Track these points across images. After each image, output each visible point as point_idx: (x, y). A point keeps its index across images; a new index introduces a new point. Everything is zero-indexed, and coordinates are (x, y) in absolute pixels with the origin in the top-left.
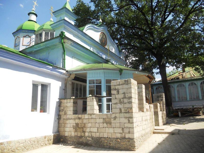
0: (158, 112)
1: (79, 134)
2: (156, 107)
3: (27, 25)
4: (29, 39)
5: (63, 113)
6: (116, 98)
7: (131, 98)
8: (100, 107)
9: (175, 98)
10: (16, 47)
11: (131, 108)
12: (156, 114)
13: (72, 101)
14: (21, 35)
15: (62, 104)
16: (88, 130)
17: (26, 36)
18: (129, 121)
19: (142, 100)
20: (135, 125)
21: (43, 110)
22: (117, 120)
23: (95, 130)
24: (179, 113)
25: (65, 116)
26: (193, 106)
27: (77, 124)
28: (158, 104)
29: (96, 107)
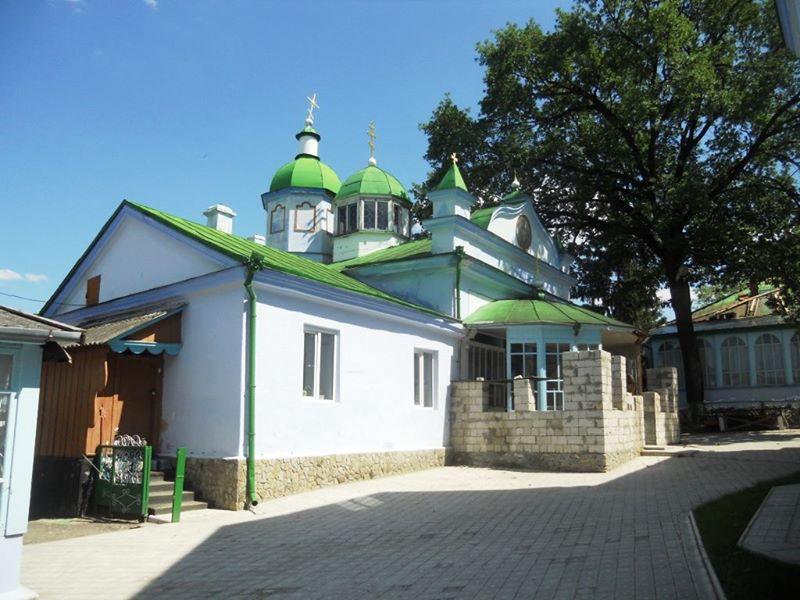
0: (656, 415)
1: (498, 448)
2: (649, 402)
3: (305, 172)
4: (312, 211)
5: (461, 409)
6: (571, 384)
7: (599, 384)
8: (537, 396)
9: (714, 377)
10: (275, 235)
11: (600, 402)
12: (650, 417)
13: (480, 385)
14: (289, 201)
15: (457, 392)
16: (516, 440)
17: (302, 206)
18: (596, 423)
19: (620, 386)
20: (606, 430)
21: (428, 403)
22: (574, 423)
23: (531, 440)
24: (721, 420)
25: (465, 415)
26: (762, 403)
27: (493, 431)
28: (657, 396)
29: (532, 399)
